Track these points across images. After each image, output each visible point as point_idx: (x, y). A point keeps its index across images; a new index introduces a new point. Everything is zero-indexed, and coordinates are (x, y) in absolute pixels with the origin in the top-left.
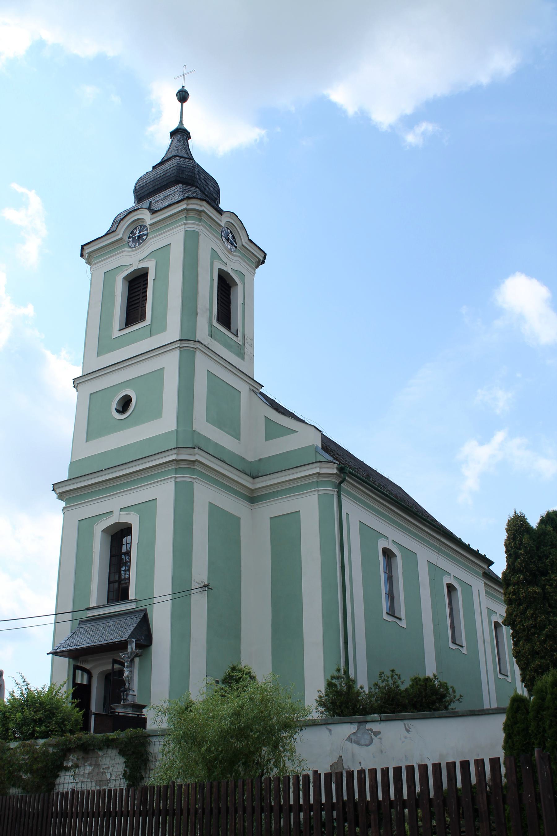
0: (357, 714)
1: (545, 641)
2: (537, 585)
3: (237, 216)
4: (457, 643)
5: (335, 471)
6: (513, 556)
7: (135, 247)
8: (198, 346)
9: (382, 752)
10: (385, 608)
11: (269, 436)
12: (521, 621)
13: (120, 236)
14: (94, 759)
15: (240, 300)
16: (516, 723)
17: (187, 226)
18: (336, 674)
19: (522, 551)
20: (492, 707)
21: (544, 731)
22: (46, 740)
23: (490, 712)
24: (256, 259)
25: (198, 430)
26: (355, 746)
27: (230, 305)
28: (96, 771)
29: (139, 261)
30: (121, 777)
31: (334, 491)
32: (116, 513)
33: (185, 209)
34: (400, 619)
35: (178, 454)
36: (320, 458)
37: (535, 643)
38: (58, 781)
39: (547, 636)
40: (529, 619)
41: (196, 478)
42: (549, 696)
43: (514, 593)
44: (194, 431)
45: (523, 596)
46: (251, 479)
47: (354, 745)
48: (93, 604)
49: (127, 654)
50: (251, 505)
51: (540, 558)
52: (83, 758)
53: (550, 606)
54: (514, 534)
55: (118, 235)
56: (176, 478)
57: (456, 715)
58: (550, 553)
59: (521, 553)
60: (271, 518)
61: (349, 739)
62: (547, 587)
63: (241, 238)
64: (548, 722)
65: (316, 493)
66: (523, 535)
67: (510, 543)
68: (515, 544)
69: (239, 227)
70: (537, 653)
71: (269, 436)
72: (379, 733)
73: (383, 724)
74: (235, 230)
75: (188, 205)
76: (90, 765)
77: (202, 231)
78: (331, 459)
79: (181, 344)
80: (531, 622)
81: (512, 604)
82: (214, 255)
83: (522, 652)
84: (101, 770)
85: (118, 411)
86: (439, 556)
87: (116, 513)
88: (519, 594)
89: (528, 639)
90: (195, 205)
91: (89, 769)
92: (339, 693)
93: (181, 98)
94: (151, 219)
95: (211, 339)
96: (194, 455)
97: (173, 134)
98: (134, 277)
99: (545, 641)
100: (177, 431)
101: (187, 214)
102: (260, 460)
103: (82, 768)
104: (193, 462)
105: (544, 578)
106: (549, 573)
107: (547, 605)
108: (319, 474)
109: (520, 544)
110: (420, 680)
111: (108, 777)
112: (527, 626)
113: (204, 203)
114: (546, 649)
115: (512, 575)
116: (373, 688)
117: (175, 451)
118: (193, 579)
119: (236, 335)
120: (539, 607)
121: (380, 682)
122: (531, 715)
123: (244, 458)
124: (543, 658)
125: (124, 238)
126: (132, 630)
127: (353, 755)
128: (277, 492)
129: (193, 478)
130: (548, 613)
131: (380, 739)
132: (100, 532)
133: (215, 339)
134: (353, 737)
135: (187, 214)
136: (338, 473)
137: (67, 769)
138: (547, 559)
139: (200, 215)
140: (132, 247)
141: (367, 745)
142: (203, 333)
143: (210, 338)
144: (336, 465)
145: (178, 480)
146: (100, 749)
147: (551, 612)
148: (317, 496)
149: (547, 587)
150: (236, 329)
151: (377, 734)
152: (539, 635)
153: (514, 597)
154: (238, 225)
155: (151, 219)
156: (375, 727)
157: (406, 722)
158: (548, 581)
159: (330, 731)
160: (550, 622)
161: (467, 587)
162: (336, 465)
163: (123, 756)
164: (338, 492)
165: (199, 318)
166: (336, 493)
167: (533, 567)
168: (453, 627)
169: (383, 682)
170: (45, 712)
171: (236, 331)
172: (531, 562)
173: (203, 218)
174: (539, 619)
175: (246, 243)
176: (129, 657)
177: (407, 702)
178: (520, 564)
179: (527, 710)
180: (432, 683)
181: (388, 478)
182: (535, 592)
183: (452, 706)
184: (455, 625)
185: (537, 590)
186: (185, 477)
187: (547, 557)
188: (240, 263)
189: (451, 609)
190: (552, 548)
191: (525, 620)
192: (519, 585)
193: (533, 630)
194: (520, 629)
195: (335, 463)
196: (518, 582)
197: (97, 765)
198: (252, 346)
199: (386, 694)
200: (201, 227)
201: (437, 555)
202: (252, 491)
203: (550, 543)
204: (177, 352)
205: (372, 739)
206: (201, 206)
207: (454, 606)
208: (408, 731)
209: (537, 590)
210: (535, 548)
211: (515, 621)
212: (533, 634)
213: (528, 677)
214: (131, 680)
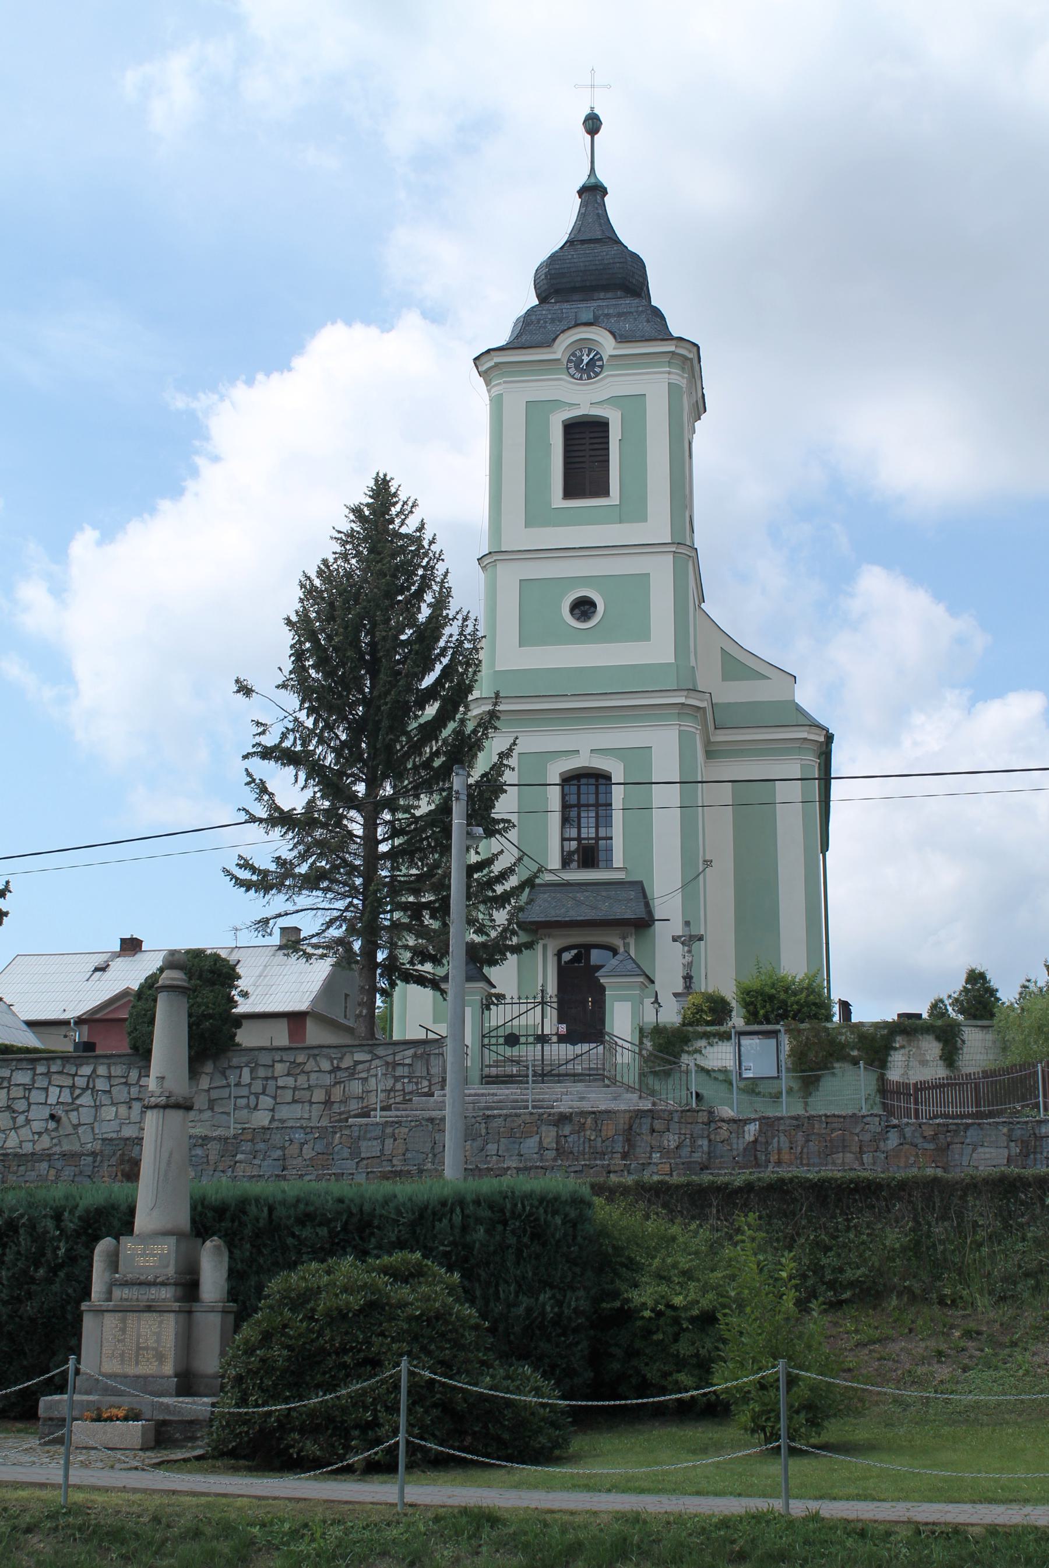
7: (581, 379)
11: (726, 677)
13: (558, 356)
17: (672, 376)
20: (274, 1044)
30: (938, 1058)
33: (673, 353)
35: (686, 697)
38: (890, 1059)
55: (555, 353)
56: (680, 725)
65: (799, 761)
71: (726, 677)
94: (614, 349)
98: (573, 421)
111: (928, 1058)
125: (562, 360)
128: (742, 750)
137: (896, 1049)
145: (682, 728)
155: (614, 349)
197: (918, 1048)
204: (671, 557)
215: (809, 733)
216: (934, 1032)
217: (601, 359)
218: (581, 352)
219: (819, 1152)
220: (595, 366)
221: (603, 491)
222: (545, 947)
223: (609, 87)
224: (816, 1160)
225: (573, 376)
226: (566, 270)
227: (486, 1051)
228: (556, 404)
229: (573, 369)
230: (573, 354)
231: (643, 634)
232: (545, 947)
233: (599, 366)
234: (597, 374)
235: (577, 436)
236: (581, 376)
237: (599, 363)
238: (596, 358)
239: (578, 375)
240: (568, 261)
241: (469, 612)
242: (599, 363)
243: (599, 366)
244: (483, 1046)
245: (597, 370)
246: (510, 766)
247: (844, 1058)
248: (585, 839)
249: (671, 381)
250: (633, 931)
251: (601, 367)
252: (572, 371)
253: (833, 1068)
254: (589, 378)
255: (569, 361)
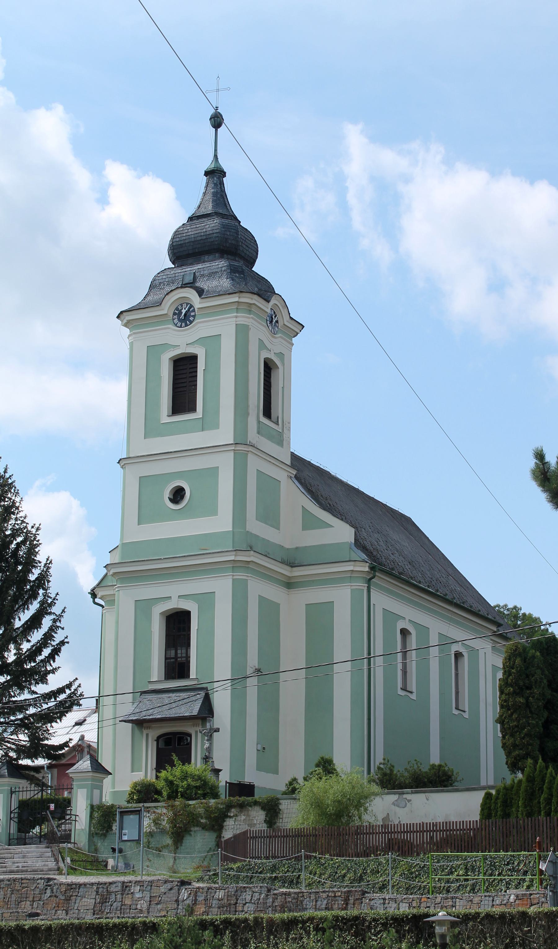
0: (396, 788)
1: (523, 738)
2: (523, 696)
3: (281, 296)
4: (460, 708)
5: (367, 569)
6: (507, 674)
7: (181, 327)
8: (251, 449)
9: (412, 811)
10: (400, 684)
11: (305, 527)
12: (508, 722)
13: (165, 312)
14: (246, 812)
15: (281, 385)
16: (486, 804)
17: (238, 319)
18: (382, 761)
19: (513, 671)
21: (497, 808)
22: (216, 800)
23: (479, 788)
24: (293, 332)
25: (250, 531)
26: (397, 808)
27: (270, 389)
28: (248, 818)
29: (187, 345)
30: (263, 822)
31: (364, 586)
32: (175, 598)
34: (411, 692)
35: (236, 555)
36: (354, 557)
37: (517, 739)
38: (225, 824)
39: (526, 735)
40: (514, 721)
41: (251, 576)
42: (501, 793)
43: (505, 701)
44: (248, 532)
45: (511, 704)
46: (289, 568)
47: (396, 807)
48: (155, 678)
49: (206, 730)
50: (287, 591)
51: (527, 676)
52: (240, 811)
53: (531, 712)
54: (510, 656)
55: (163, 310)
56: (233, 575)
57: (457, 790)
58: (536, 673)
59: (513, 672)
60: (306, 604)
61: (394, 804)
62: (530, 698)
63: (282, 315)
64: (499, 805)
65: (349, 587)
66: (516, 657)
67: (506, 663)
68: (510, 663)
69: (282, 306)
70: (517, 746)
71: (305, 527)
72: (410, 800)
73: (413, 795)
74: (277, 308)
75: (239, 298)
76: (244, 815)
77: (253, 325)
78: (364, 556)
79: (235, 447)
80: (515, 723)
81: (503, 708)
82: (262, 345)
83: (507, 744)
84: (251, 818)
85: (171, 500)
86: (450, 626)
87: (175, 598)
88: (509, 702)
89: (512, 735)
90: (247, 299)
91: (243, 817)
92: (385, 774)
93: (216, 125)
94: (200, 303)
95: (259, 436)
96: (249, 556)
97: (207, 173)
98: (182, 357)
99: (523, 738)
100: (233, 532)
101: (238, 305)
102: (297, 548)
103: (239, 817)
104: (248, 562)
105: (528, 692)
106: (533, 688)
107: (528, 712)
108: (352, 571)
109: (514, 664)
110: (435, 765)
111: (255, 822)
112: (512, 726)
113: (256, 297)
114: (524, 743)
115: (506, 687)
116: (404, 771)
117: (234, 553)
118: (248, 665)
119: (277, 423)
120: (522, 713)
121: (408, 767)
122: (493, 801)
123: (283, 546)
124: (521, 749)
125: (169, 314)
126: (199, 707)
127: (395, 813)
128: (313, 581)
129: (248, 576)
130: (529, 717)
131: (411, 804)
132: (159, 614)
133: (262, 435)
134: (396, 803)
135: (238, 305)
136: (369, 571)
137: (230, 817)
138: (532, 677)
139: (250, 307)
140: (177, 325)
141: (403, 808)
142: (252, 435)
143: (257, 435)
144: (368, 564)
145: (235, 577)
146: (251, 806)
147: (530, 717)
148: (350, 590)
149: (530, 698)
150: (277, 417)
151: (409, 801)
152: (520, 733)
153: (505, 704)
154: (281, 304)
155: (200, 303)
156: (408, 797)
157: (427, 794)
158: (531, 693)
159: (383, 799)
160: (529, 724)
161: (474, 652)
162: (368, 564)
163: (264, 810)
164: (368, 587)
165: (249, 419)
166: (366, 588)
167: (521, 683)
168: (457, 693)
169: (410, 767)
170: (201, 781)
171: (277, 418)
172: (519, 679)
173: (252, 309)
174: (521, 722)
175: (287, 321)
176: (208, 733)
177: (426, 780)
178: (512, 680)
179: (492, 798)
180: (443, 768)
181: (397, 509)
182: (520, 702)
183: (456, 784)
184: (460, 690)
185: (522, 700)
186: (240, 575)
187: (533, 676)
188: (281, 344)
189: (457, 675)
190: (538, 669)
191: (511, 721)
192: (509, 695)
193: (516, 729)
194: (507, 727)
195: (367, 562)
196: (509, 693)
197: (248, 815)
198: (289, 430)
199: (413, 775)
200: (251, 320)
201: (448, 625)
202: (290, 578)
203: (536, 665)
204: (232, 454)
205: (406, 804)
206: (252, 299)
207: (460, 672)
208: (427, 799)
209: (522, 700)
210: (524, 669)
211: (504, 721)
212: (516, 732)
213: (509, 762)
214: (211, 750)
215: (354, 566)
216: (260, 805)
217: (194, 311)
218: (182, 306)
219: (15, 900)
220: (190, 316)
221: (192, 408)
222: (147, 735)
223: (229, 89)
224: (14, 906)
225: (176, 325)
226: (182, 242)
227: (12, 822)
228: (165, 347)
229: (176, 320)
230: (177, 309)
231: (213, 511)
232: (147, 735)
233: (193, 316)
234: (191, 322)
235: (181, 368)
236: (181, 324)
237: (193, 314)
238: (191, 310)
239: (179, 324)
240: (184, 235)
241: (40, 525)
242: (193, 314)
243: (193, 316)
244: (11, 819)
245: (191, 319)
246: (61, 627)
247: (198, 824)
248: (179, 658)
249: (238, 323)
250: (200, 722)
251: (194, 316)
252: (176, 321)
253: (191, 831)
254: (186, 325)
255: (174, 314)
